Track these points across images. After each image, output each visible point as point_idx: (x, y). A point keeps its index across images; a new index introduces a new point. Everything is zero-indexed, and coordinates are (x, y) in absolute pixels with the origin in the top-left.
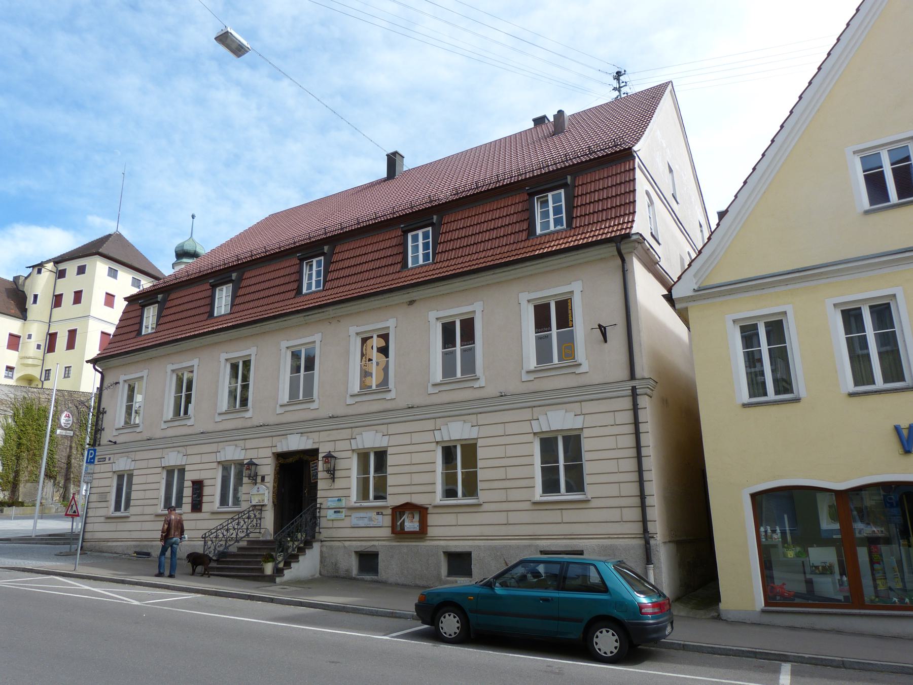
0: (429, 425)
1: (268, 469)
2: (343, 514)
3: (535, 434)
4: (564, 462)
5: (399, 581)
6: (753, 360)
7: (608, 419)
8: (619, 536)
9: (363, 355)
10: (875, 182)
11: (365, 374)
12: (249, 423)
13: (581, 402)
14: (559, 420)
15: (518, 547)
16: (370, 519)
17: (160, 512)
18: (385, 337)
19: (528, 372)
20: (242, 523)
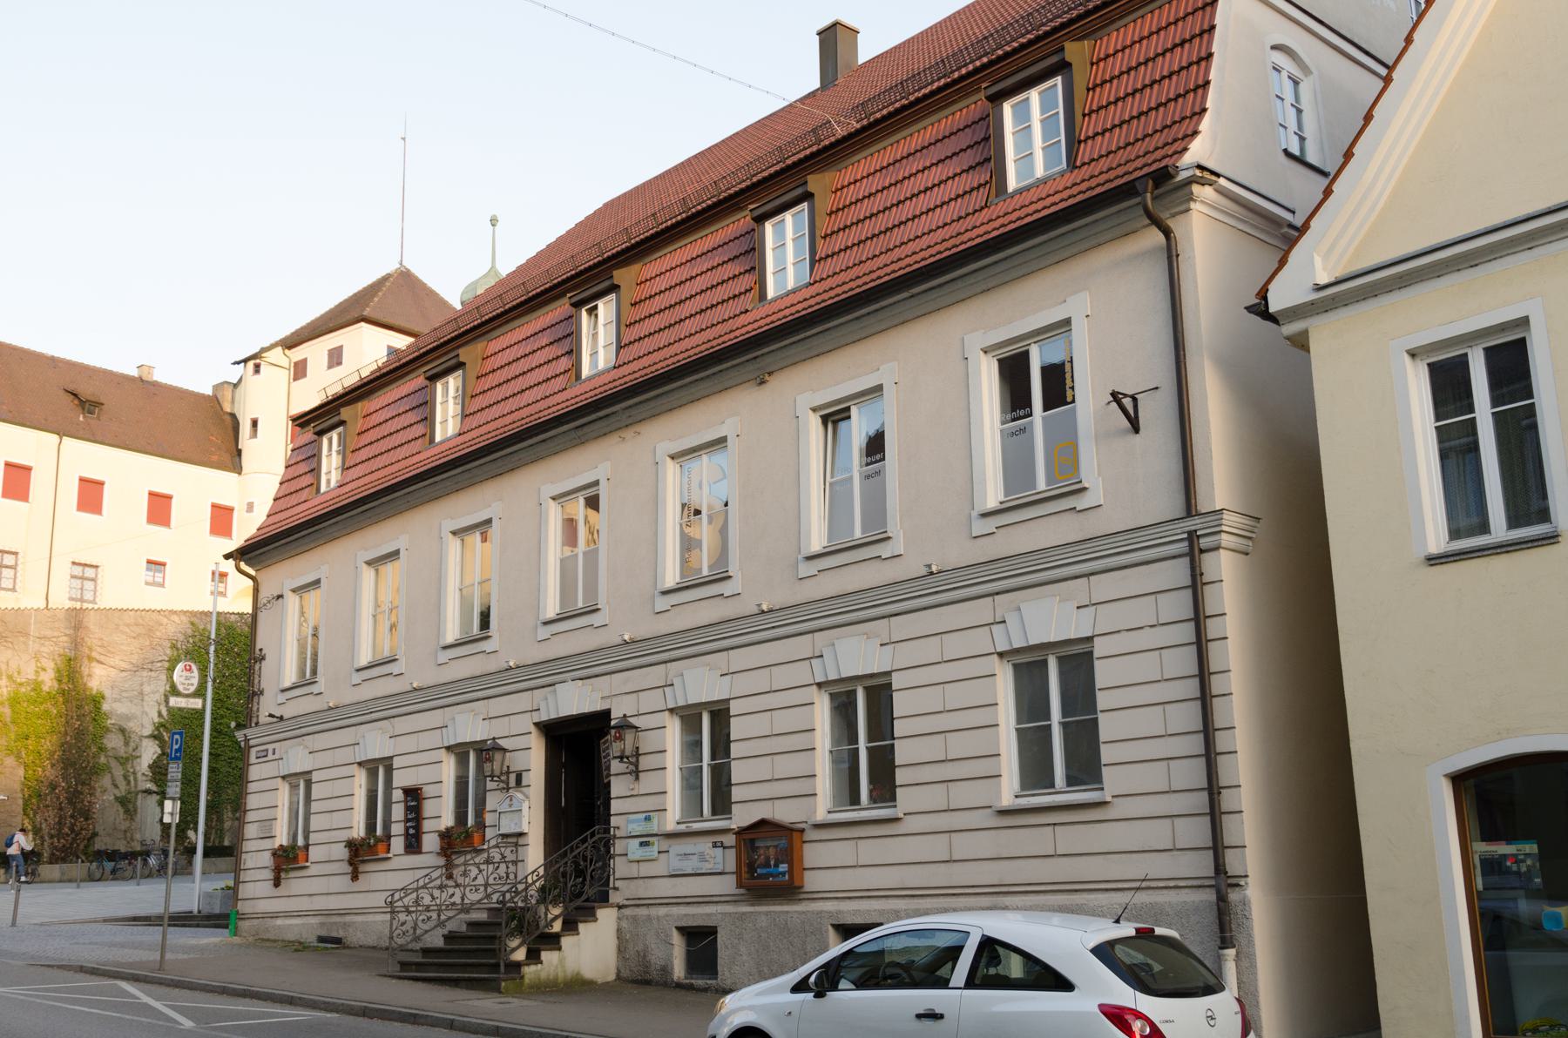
0: (980, 611)
1: (533, 759)
2: (655, 848)
3: (1001, 655)
6: (1457, 450)
10: (153, 584)
12: (492, 665)
14: (1048, 618)
16: (703, 859)
17: (1007, 800)
19: (985, 515)
20: (474, 871)
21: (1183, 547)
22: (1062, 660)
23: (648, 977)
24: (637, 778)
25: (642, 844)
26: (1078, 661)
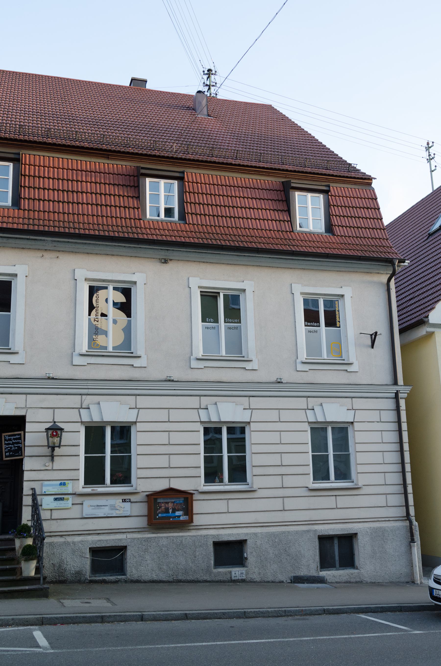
0: (194, 402)
2: (70, 502)
4: (331, 451)
5: (155, 578)
7: (375, 416)
8: (388, 519)
9: (91, 307)
11: (95, 331)
13: (352, 398)
14: (335, 412)
15: (297, 532)
18: (127, 292)
21: (393, 395)
22: (333, 428)
23: (62, 578)
24: (52, 460)
25: (56, 499)
26: (342, 432)
